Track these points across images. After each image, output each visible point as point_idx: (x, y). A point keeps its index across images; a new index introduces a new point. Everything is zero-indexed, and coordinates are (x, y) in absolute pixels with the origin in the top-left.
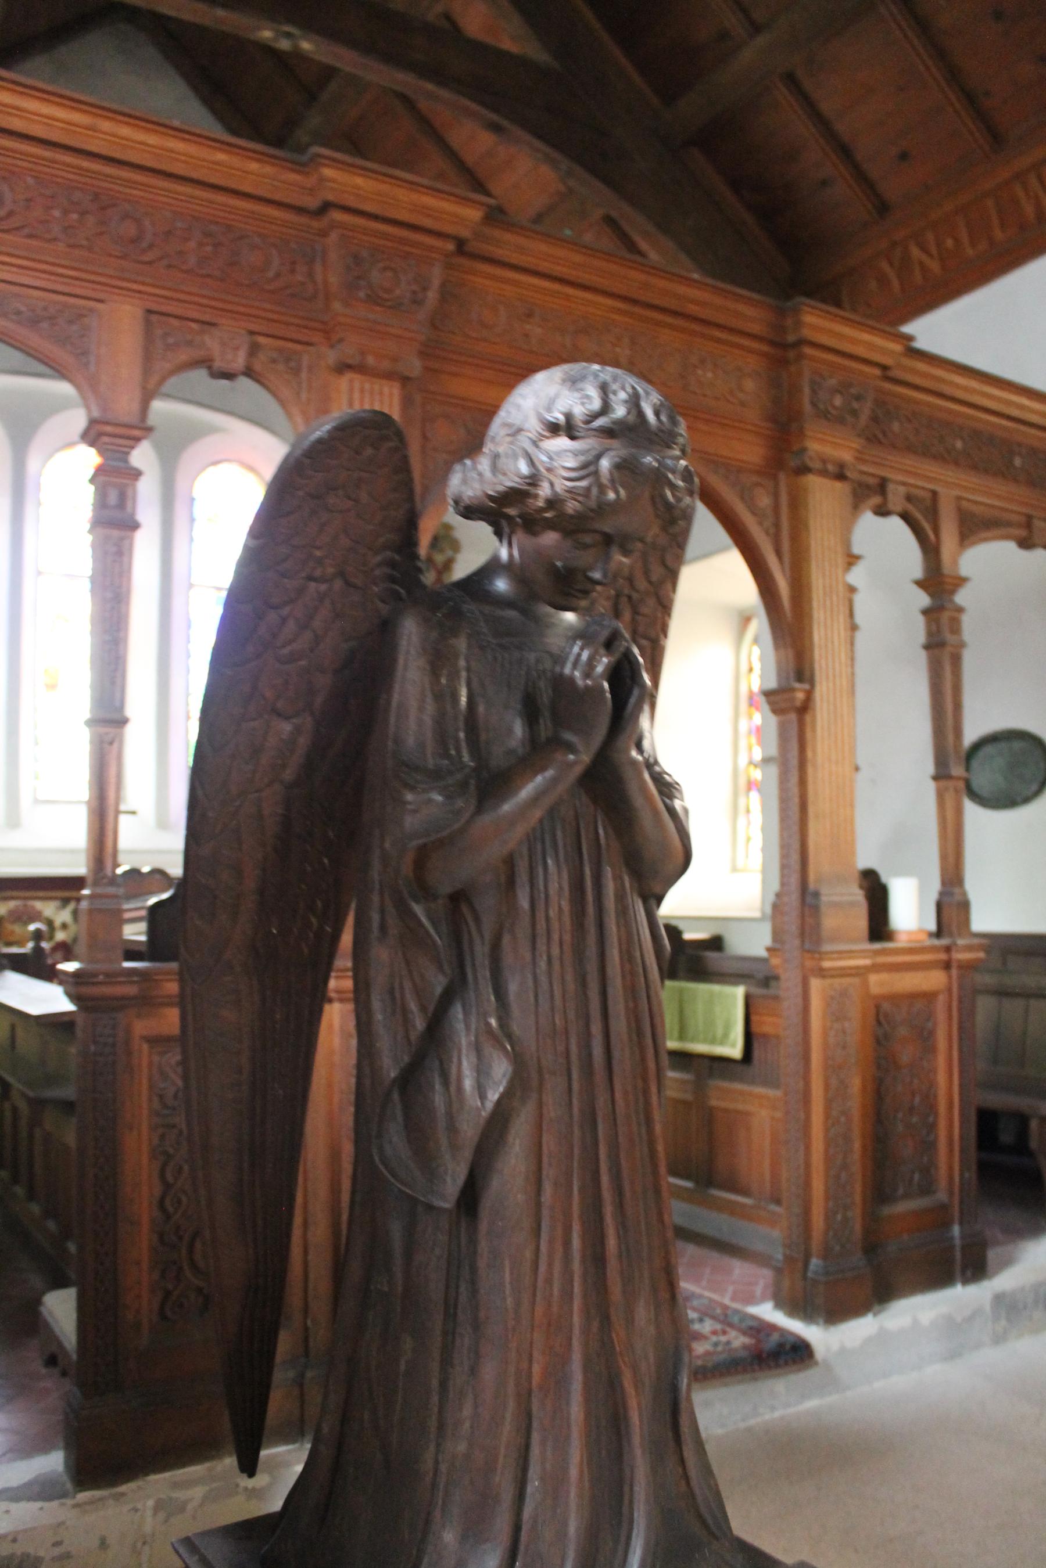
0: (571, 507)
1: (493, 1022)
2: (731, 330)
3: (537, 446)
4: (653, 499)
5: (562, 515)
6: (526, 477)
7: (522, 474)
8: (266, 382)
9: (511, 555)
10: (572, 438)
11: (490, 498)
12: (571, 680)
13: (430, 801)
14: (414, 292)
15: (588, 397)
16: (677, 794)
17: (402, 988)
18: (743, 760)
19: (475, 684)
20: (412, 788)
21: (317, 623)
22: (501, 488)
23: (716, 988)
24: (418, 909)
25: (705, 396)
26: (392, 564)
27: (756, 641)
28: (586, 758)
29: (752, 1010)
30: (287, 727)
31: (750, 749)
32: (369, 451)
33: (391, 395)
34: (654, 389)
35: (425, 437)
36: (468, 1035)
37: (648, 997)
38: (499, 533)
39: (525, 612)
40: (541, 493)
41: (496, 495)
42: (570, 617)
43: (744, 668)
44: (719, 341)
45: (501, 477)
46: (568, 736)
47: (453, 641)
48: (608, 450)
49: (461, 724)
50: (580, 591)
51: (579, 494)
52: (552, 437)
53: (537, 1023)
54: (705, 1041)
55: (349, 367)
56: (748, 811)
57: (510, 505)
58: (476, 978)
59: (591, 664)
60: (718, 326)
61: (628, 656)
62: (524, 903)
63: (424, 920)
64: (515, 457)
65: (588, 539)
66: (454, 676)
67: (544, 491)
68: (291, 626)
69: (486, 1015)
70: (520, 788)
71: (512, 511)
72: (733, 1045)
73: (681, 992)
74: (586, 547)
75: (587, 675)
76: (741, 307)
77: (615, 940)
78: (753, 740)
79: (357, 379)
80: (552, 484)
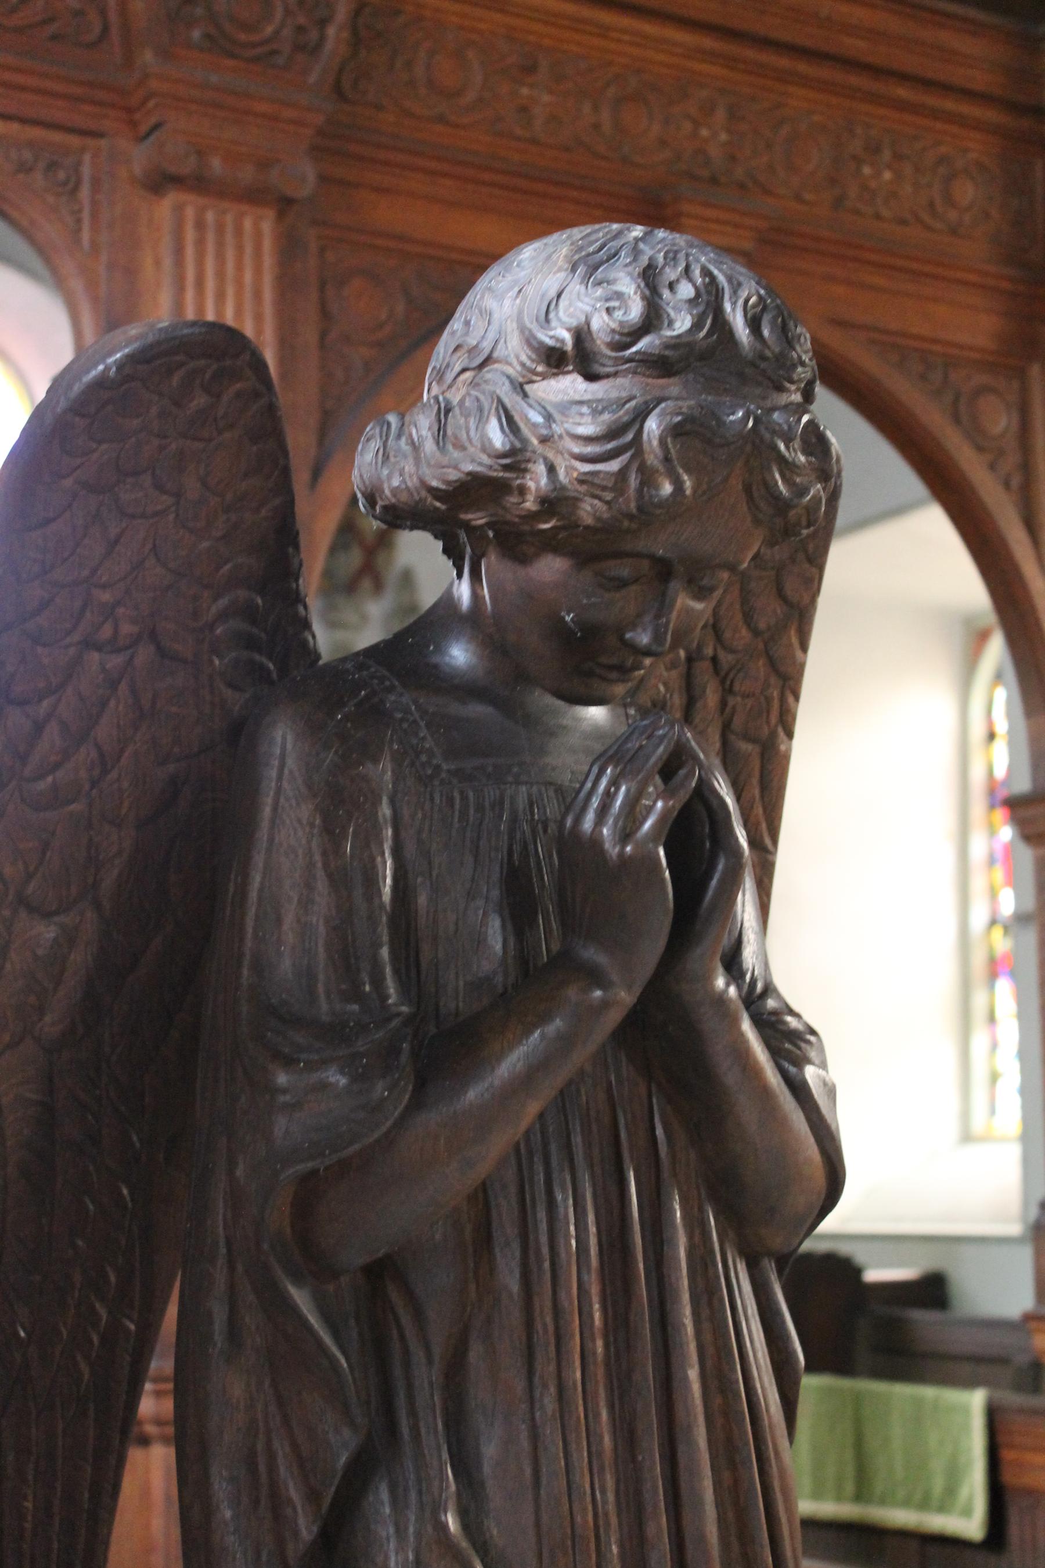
0: (589, 510)
1: (452, 1522)
2: (927, 84)
3: (525, 395)
4: (748, 489)
5: (572, 525)
6: (504, 455)
7: (497, 450)
8: (15, 214)
9: (476, 596)
10: (591, 377)
11: (433, 491)
12: (595, 843)
13: (324, 1086)
14: (300, 29)
15: (619, 296)
16: (813, 1054)
17: (272, 1457)
18: (979, 917)
19: (410, 849)
20: (289, 1062)
21: (104, 731)
22: (453, 475)
23: (928, 1392)
24: (300, 1297)
25: (878, 217)
26: (249, 613)
27: (998, 678)
28: (626, 997)
29: (1001, 1439)
30: (47, 932)
31: (993, 894)
32: (200, 400)
33: (258, 235)
34: (752, 275)
35: (325, 313)
36: (401, 1549)
37: (761, 1459)
38: (452, 551)
39: (507, 707)
40: (531, 485)
41: (443, 487)
42: (596, 714)
43: (977, 730)
44: (902, 106)
45: (456, 454)
46: (592, 954)
47: (368, 769)
48: (659, 401)
49: (384, 934)
50: (611, 668)
51: (604, 488)
52: (555, 375)
53: (538, 1524)
54: (906, 1503)
55: (176, 181)
56: (992, 1019)
57: (473, 505)
58: (415, 1430)
59: (633, 815)
60: (903, 77)
61: (704, 794)
62: (511, 1281)
63: (313, 1320)
64: (482, 420)
65: (623, 570)
66: (369, 838)
67: (537, 480)
68: (52, 736)
69: (438, 1508)
70: (500, 1057)
71: (478, 519)
72: (967, 1512)
73: (858, 1400)
74: (622, 584)
75: (625, 836)
76: (946, 37)
77: (692, 1347)
78: (999, 874)
79: (191, 204)
80: (551, 469)
